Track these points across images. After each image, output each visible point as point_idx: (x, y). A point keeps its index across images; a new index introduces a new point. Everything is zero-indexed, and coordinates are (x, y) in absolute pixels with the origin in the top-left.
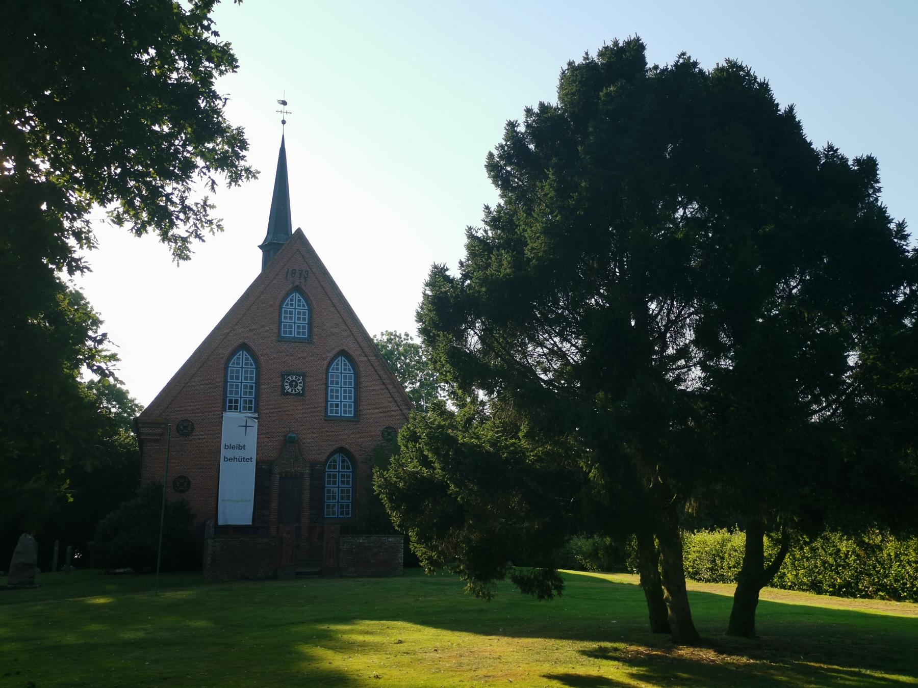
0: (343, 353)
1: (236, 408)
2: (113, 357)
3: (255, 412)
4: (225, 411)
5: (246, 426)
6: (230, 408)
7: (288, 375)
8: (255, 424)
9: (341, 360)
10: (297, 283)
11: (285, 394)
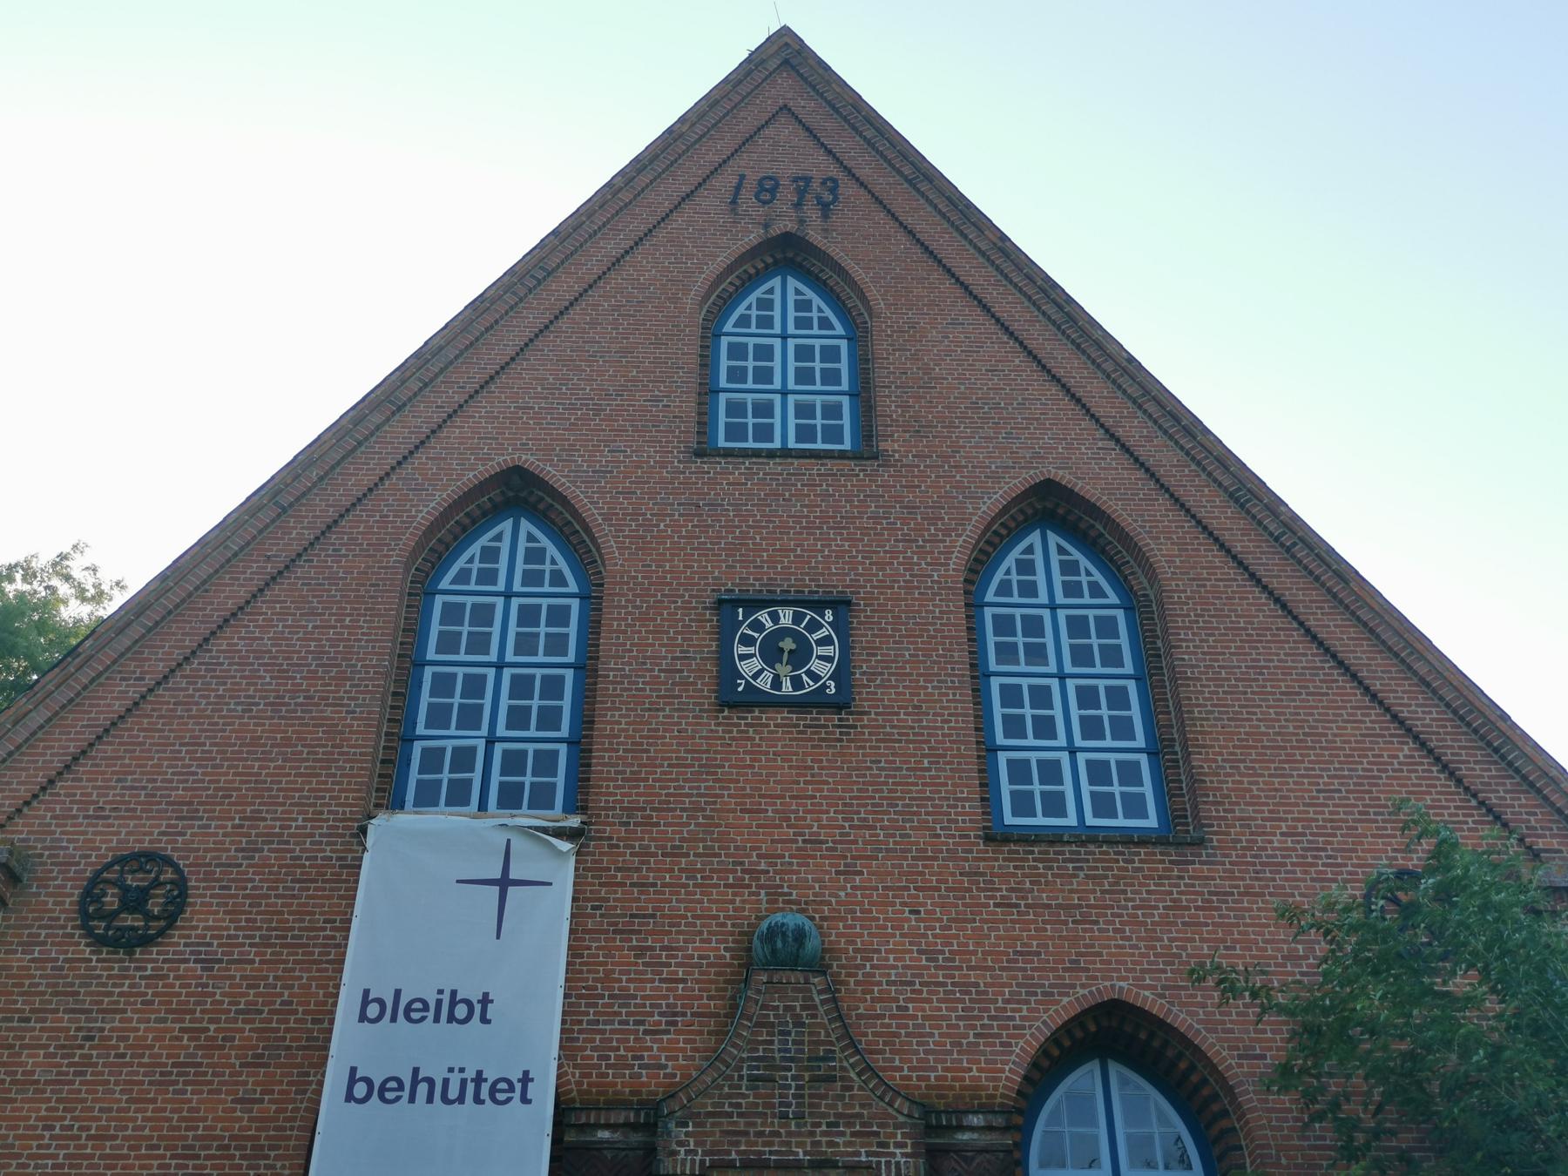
0: (1051, 507)
1: (459, 796)
2: (398, 993)
3: (569, 809)
4: (398, 805)
5: (504, 883)
6: (427, 797)
7: (754, 605)
8: (558, 870)
9: (1044, 550)
10: (785, 224)
11: (735, 699)
